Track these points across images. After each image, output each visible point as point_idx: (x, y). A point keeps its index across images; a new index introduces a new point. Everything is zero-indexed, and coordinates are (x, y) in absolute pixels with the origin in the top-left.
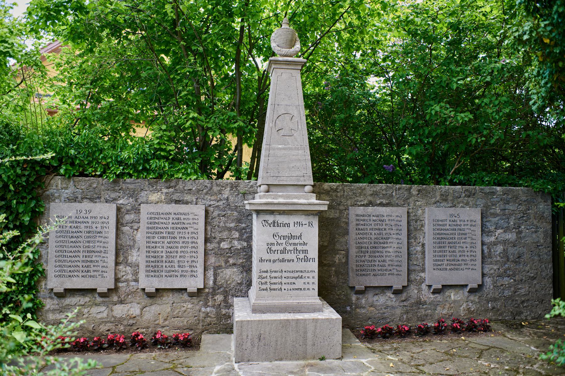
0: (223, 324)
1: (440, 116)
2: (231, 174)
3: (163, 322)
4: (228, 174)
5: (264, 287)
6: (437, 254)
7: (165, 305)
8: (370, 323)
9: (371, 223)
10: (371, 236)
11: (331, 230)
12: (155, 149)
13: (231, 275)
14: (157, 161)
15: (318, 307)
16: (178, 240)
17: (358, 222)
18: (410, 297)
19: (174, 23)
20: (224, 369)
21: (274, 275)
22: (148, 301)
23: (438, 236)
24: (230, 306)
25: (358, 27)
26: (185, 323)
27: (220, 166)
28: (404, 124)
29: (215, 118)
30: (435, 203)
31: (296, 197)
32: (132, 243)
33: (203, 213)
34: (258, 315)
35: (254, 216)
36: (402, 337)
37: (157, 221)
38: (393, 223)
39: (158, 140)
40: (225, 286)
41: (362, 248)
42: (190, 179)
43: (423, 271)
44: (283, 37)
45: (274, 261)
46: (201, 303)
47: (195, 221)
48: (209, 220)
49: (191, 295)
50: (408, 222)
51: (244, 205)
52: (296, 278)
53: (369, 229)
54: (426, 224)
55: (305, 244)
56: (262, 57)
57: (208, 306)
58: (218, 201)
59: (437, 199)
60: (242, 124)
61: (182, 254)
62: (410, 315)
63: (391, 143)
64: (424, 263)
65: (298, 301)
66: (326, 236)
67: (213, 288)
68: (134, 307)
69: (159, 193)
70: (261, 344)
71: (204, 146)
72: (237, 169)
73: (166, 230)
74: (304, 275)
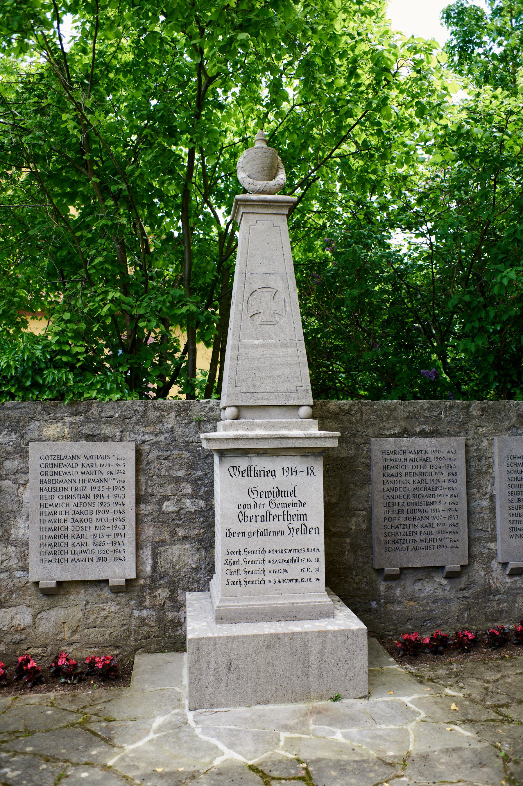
0: (170, 637)
1: (517, 286)
2: (180, 389)
3: (71, 637)
4: (174, 390)
5: (235, 578)
6: (515, 511)
7: (72, 609)
8: (410, 627)
9: (407, 463)
10: (408, 485)
11: (344, 478)
12: (54, 351)
13: (181, 555)
14: (55, 372)
15: (326, 609)
16: (91, 500)
17: (386, 464)
18: (473, 582)
19: (80, 149)
20: (170, 723)
21: (250, 557)
22: (45, 602)
23: (516, 483)
24: (179, 606)
25: (378, 149)
26: (107, 636)
27: (161, 377)
28: (456, 303)
29: (150, 299)
30: (509, 429)
31: (285, 427)
32: (16, 508)
33: (132, 455)
34: (226, 626)
35: (216, 459)
36: (464, 651)
37: (56, 469)
38: (442, 463)
39: (58, 337)
40: (171, 574)
41: (393, 505)
42: (111, 399)
43: (493, 539)
44: (257, 162)
45: (251, 535)
46: (133, 602)
47: (119, 468)
48: (143, 466)
49: (116, 590)
50: (467, 461)
51: (199, 441)
52: (288, 562)
53: (403, 474)
54: (496, 463)
55: (301, 504)
56: (224, 208)
57: (145, 607)
58: (156, 435)
59: (513, 422)
60: (193, 308)
61: (100, 524)
62: (474, 613)
63: (430, 336)
64: (495, 527)
65: (293, 601)
66: (335, 488)
67: (151, 577)
68: (23, 613)
69: (60, 424)
70: (233, 676)
71: (136, 346)
72: (188, 381)
73: (71, 485)
74: (301, 556)
